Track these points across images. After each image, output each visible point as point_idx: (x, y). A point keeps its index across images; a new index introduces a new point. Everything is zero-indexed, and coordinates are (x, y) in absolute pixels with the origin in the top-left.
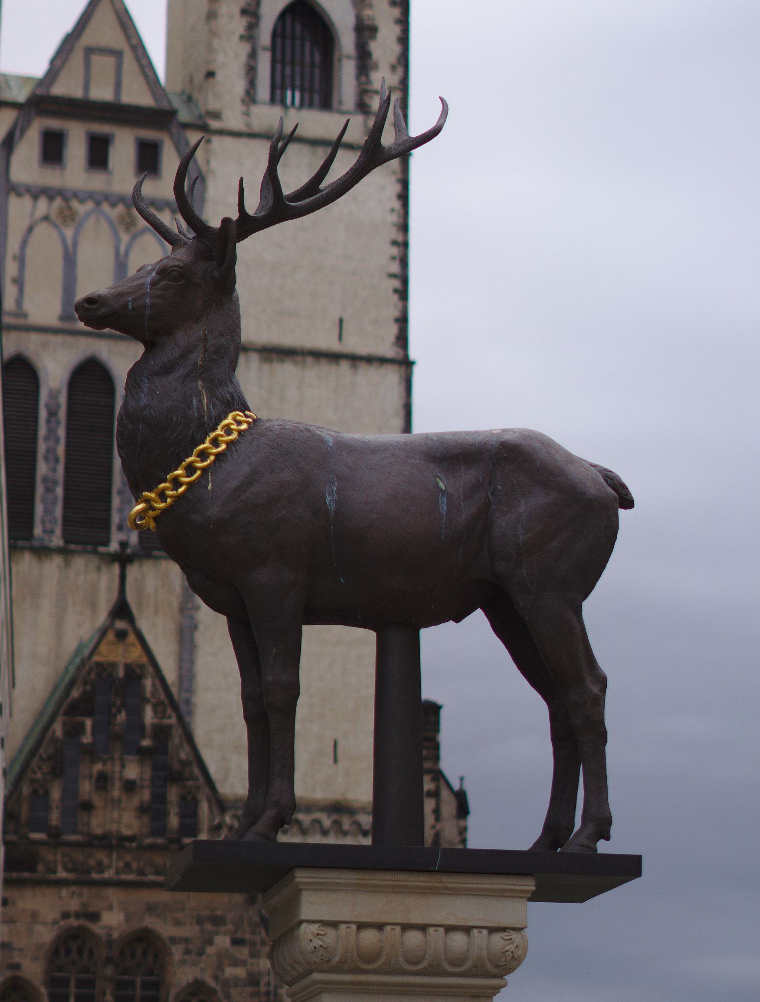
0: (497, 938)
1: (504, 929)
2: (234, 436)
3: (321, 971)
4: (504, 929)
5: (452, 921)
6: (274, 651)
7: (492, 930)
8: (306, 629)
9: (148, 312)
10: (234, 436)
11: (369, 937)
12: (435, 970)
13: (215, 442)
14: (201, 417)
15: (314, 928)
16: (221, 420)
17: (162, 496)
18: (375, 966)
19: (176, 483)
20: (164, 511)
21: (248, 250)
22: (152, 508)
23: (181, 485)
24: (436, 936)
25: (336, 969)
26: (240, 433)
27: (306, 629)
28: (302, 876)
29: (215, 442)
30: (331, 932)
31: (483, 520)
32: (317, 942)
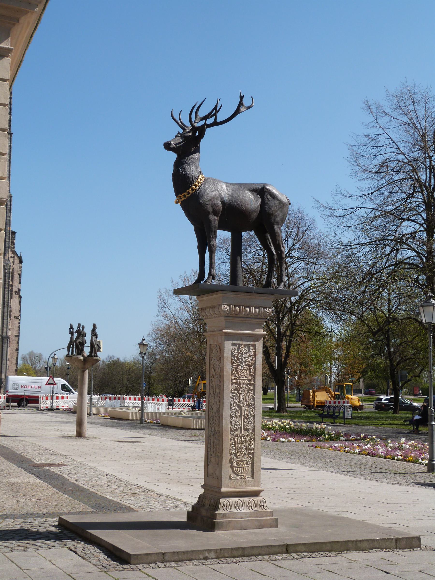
21: (208, 131)
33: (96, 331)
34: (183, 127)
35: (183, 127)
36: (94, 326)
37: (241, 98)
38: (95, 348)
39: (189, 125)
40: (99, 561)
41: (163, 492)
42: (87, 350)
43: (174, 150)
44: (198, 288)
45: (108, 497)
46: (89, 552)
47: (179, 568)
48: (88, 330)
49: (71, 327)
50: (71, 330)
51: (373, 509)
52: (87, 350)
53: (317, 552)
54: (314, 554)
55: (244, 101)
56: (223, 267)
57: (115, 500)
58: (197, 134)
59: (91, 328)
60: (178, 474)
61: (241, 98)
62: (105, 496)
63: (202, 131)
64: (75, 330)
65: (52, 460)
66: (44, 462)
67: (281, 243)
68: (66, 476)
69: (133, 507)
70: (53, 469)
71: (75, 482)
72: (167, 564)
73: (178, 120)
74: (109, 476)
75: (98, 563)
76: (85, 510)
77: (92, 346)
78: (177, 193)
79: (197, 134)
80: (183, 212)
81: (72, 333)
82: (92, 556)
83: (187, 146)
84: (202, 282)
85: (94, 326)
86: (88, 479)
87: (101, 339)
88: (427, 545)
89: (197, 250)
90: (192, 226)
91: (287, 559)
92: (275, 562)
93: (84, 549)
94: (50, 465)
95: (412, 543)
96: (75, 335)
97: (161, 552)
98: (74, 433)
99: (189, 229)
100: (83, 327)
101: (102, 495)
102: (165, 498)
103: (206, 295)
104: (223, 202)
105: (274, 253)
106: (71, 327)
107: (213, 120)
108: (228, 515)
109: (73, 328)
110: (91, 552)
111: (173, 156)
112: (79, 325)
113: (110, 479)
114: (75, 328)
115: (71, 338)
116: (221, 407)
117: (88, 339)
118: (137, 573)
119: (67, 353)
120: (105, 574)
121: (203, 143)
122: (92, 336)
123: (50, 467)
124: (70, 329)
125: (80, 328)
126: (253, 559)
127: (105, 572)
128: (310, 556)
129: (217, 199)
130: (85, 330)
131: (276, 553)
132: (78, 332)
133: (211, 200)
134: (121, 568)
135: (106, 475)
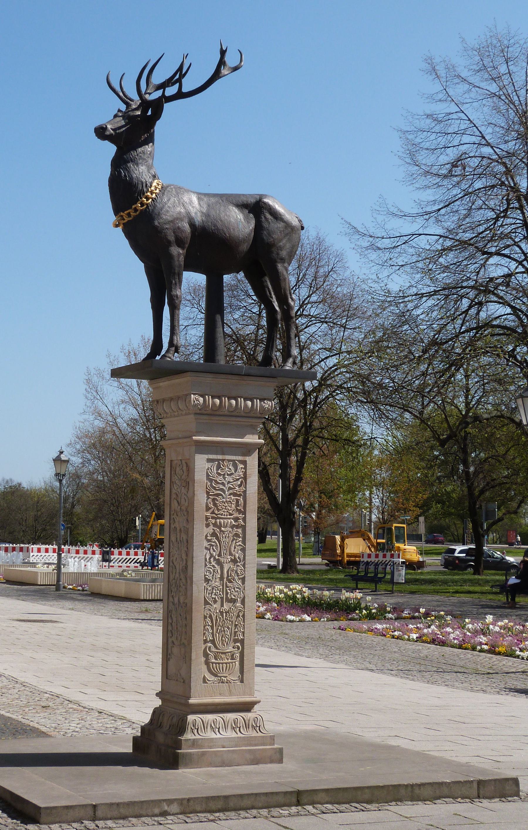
17: (384, 556)
24: (150, 823)
34: (126, 100)
37: (223, 53)
39: (135, 96)
43: (111, 138)
44: (152, 366)
54: (343, 807)
55: (227, 59)
58: (149, 113)
61: (223, 53)
63: (157, 107)
67: (288, 292)
73: (118, 89)
79: (149, 113)
84: (158, 358)
91: (298, 814)
99: (138, 268)
103: (164, 379)
128: (335, 810)
129: (182, 220)
131: (280, 806)
133: (172, 221)
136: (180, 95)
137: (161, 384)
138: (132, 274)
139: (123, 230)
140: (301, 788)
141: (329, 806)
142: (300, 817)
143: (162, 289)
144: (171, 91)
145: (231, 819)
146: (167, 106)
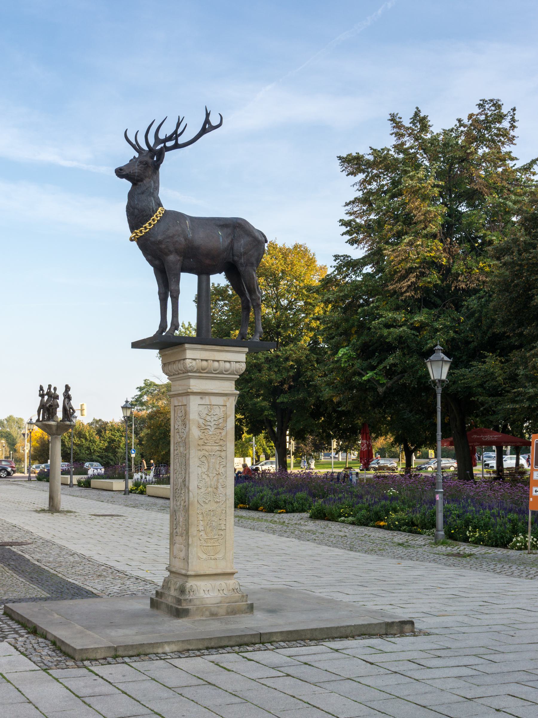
0: (238, 364)
1: (239, 362)
2: (159, 218)
3: (191, 372)
4: (239, 362)
5: (226, 360)
6: (371, 299)
7: (236, 362)
8: (181, 273)
9: (136, 174)
10: (161, 215)
11: (204, 363)
12: (221, 373)
13: (154, 220)
14: (153, 208)
15: (190, 360)
16: (151, 217)
17: (141, 232)
18: (205, 371)
19: (146, 228)
20: (141, 236)
21: (168, 155)
22: (137, 235)
23: (147, 229)
24: (222, 363)
25: (195, 372)
26: (158, 220)
27: (181, 273)
28: (187, 346)
29: (150, 224)
30: (194, 362)
31: (231, 247)
32: (190, 365)
33: (70, 393)
34: (138, 149)
35: (138, 149)
36: (67, 388)
37: (208, 115)
38: (68, 413)
39: (145, 148)
40: (41, 657)
41: (135, 573)
42: (60, 414)
43: (128, 177)
44: (165, 342)
45: (70, 580)
46: (30, 646)
47: (133, 664)
48: (60, 392)
49: (41, 388)
50: (41, 392)
51: (367, 589)
52: (60, 414)
53: (296, 641)
54: (290, 644)
55: (211, 118)
56: (188, 315)
57: (76, 583)
58: (155, 159)
59: (64, 390)
60: (156, 551)
61: (208, 115)
62: (67, 579)
63: (160, 155)
64: (45, 392)
65: (16, 537)
66: (6, 540)
67: (256, 287)
68: (27, 556)
69: (95, 591)
70: (14, 549)
71: (36, 563)
72: (120, 660)
73: (134, 143)
74: (76, 555)
75: (39, 659)
76: (39, 596)
77: (65, 410)
78: (133, 227)
79: (155, 159)
80: (140, 252)
81: (42, 396)
82: (33, 651)
83: (142, 172)
84: (164, 334)
85: (67, 388)
86: (51, 559)
87: (75, 404)
88: (422, 628)
89: (157, 297)
90: (153, 268)
91: (259, 650)
92: (245, 654)
93: (26, 643)
94: (11, 544)
95: (403, 627)
96: (46, 398)
97: (113, 645)
98: (46, 506)
99: (148, 271)
100: (55, 389)
101: (64, 577)
102: (135, 580)
103: (168, 349)
104: (186, 239)
105: (249, 299)
106: (41, 388)
107: (174, 141)
108: (195, 600)
109: (43, 391)
110: (33, 647)
111: (127, 185)
112: (50, 386)
113: (77, 559)
114: (46, 390)
115: (41, 401)
116: (187, 478)
117: (60, 401)
118: (84, 671)
119: (37, 418)
120: (44, 673)
121: (163, 169)
122: (65, 399)
123: (11, 546)
124: (40, 391)
125: (50, 389)
126: (220, 652)
127: (45, 670)
128: (286, 646)
129: (179, 236)
130: (58, 392)
131: (247, 645)
132: (48, 394)
133: (172, 237)
134: (64, 665)
135: (74, 554)
136: (177, 146)
137: (167, 352)
138: (144, 277)
139: (138, 244)
140: (261, 632)
141: (282, 644)
142: (260, 652)
143: (168, 289)
144: (169, 144)
145: (212, 654)
146: (166, 154)
